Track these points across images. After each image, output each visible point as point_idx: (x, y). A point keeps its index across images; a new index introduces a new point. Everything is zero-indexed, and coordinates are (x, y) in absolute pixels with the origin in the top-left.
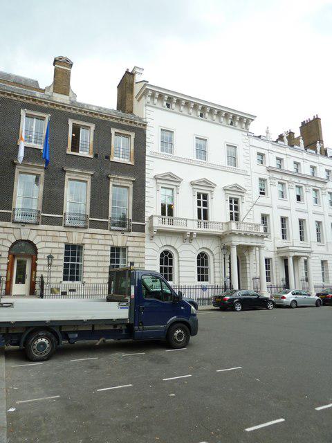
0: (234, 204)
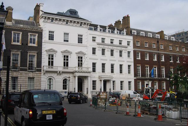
0: (80, 59)
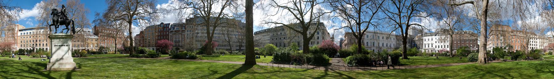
0: (432, 45)
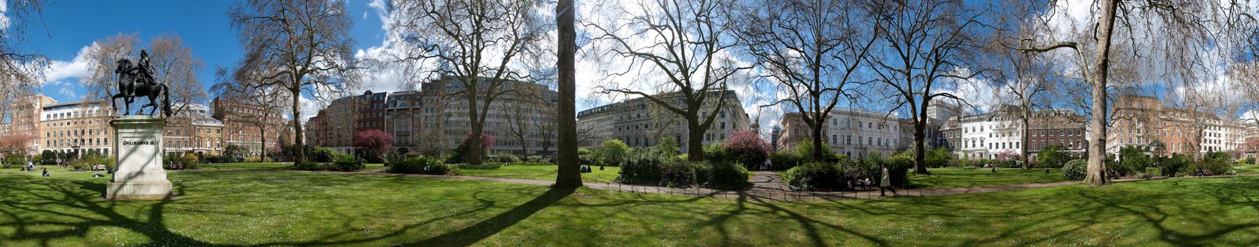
0: (982, 141)
